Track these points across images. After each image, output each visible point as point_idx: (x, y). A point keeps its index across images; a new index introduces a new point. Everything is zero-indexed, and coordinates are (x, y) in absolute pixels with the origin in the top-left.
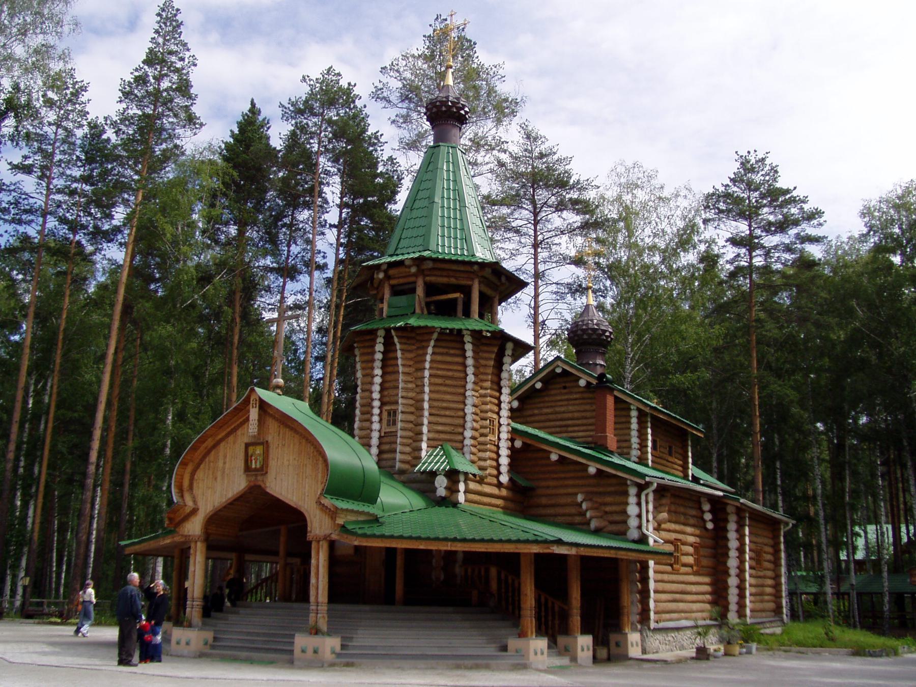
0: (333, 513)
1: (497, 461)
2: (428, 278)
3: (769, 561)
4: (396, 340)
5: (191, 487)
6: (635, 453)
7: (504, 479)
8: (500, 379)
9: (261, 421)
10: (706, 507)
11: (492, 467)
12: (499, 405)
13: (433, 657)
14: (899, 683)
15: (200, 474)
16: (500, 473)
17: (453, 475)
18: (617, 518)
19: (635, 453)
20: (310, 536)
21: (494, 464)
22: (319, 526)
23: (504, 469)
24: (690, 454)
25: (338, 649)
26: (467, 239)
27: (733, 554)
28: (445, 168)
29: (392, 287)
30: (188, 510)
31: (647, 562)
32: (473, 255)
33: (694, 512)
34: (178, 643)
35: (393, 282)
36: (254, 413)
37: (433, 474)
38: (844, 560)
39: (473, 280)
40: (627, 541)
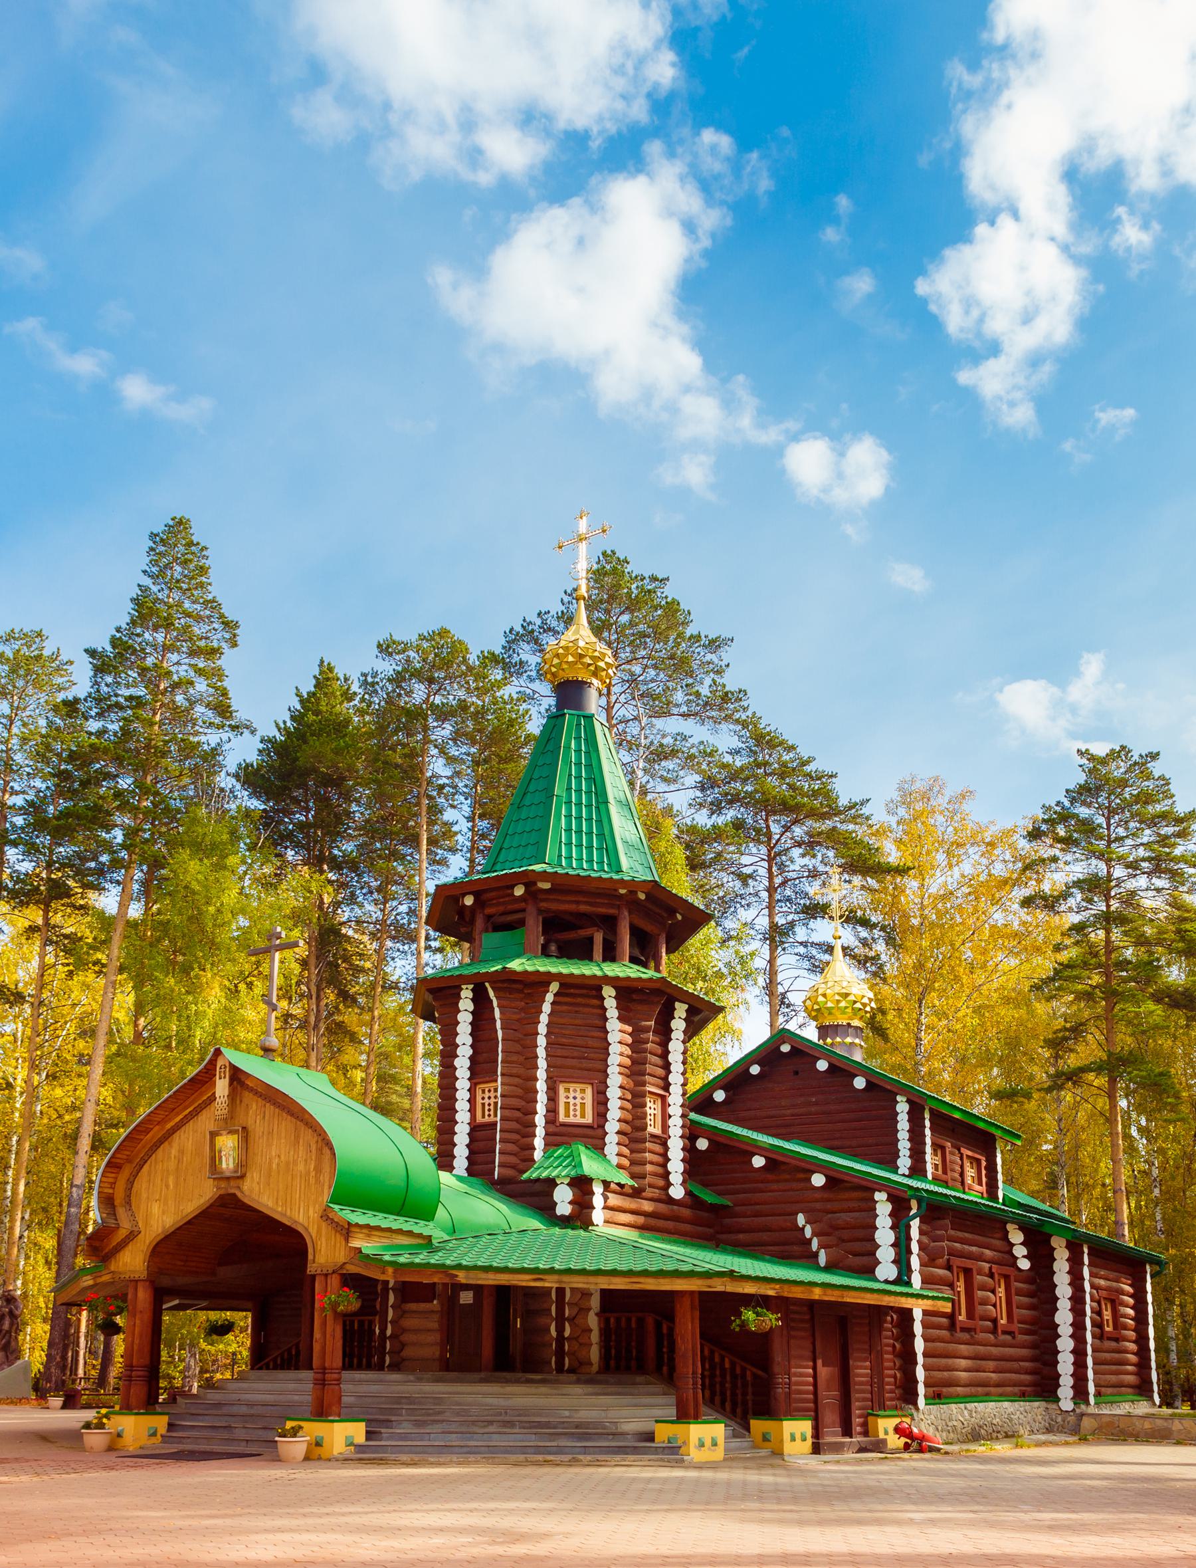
0: (347, 1230)
1: (664, 1166)
2: (544, 905)
3: (1126, 1316)
4: (491, 993)
5: (128, 1202)
6: (904, 1162)
7: (677, 1192)
9: (233, 1096)
10: (1016, 1237)
11: (655, 1174)
12: (666, 1087)
15: (141, 1184)
16: (669, 1184)
17: (581, 1184)
18: (857, 1246)
19: (904, 1162)
20: (311, 1269)
21: (660, 1170)
22: (325, 1253)
23: (676, 1178)
24: (927, 1123)
25: (360, 1439)
28: (573, 746)
29: (489, 918)
30: (122, 1233)
32: (620, 871)
33: (997, 1243)
34: (793, 1439)
35: (488, 911)
36: (222, 1087)
37: (551, 1183)
39: (619, 907)
40: (877, 1280)
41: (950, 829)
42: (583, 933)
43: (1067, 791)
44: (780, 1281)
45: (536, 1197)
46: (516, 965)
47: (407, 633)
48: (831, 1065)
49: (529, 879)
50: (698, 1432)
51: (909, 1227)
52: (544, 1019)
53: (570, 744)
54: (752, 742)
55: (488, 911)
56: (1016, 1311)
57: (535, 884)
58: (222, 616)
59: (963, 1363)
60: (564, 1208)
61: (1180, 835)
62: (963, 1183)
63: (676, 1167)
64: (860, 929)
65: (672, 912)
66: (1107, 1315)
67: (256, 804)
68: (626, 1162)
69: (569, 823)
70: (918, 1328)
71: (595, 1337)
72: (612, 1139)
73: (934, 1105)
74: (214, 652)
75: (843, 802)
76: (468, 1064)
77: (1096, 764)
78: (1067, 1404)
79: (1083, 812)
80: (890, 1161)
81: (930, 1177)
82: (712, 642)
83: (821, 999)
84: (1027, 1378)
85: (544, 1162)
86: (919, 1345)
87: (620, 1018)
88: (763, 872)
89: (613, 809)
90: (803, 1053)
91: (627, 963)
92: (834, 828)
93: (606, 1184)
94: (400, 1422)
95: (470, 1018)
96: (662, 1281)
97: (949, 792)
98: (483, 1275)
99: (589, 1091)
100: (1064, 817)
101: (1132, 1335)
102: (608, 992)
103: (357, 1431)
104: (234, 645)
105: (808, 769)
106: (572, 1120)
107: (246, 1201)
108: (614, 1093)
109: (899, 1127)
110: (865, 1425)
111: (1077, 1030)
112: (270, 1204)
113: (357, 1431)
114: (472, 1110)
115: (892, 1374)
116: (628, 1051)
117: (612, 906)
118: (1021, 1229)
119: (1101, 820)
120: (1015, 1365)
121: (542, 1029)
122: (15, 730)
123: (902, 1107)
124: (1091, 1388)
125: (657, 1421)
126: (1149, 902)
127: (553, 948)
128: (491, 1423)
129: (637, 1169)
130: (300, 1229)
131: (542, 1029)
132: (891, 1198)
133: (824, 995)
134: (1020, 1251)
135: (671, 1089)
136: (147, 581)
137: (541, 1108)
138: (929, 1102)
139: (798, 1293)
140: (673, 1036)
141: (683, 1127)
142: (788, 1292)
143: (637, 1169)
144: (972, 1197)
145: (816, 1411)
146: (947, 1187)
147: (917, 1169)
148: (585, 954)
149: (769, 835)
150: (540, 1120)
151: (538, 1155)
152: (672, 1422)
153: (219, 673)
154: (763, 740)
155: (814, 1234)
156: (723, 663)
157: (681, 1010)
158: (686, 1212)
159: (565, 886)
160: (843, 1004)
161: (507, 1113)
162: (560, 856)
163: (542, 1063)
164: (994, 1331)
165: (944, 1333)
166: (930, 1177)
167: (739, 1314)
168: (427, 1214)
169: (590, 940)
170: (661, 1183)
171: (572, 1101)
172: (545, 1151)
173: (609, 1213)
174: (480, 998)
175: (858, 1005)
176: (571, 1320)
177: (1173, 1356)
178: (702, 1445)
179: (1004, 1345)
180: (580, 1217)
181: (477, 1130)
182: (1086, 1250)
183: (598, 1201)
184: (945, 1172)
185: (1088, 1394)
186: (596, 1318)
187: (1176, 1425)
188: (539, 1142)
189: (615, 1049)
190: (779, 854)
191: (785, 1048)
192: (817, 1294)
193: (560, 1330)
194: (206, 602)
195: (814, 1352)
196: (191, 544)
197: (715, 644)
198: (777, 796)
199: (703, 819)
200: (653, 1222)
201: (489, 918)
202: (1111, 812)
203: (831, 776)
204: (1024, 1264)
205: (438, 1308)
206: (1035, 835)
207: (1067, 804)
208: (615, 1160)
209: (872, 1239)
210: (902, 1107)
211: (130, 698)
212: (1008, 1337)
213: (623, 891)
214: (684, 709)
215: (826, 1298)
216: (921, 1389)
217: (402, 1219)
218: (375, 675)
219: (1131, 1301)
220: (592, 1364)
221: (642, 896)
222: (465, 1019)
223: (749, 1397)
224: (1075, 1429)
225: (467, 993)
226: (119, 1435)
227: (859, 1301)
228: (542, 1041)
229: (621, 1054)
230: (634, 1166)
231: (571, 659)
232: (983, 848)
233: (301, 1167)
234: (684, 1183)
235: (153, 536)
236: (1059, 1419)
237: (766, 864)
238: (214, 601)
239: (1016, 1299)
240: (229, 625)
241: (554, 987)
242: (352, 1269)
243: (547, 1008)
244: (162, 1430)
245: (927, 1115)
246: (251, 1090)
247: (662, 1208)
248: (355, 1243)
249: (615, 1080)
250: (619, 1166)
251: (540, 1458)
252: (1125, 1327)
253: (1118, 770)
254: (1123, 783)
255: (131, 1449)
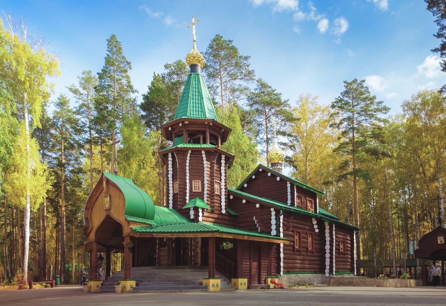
0: (129, 222)
1: (220, 204)
2: (187, 128)
6: (289, 202)
7: (224, 212)
8: (221, 170)
10: (315, 222)
11: (218, 206)
13: (167, 289)
14: (377, 304)
17: (196, 209)
19: (289, 202)
20: (124, 235)
22: (126, 231)
23: (223, 207)
24: (295, 190)
25: (134, 286)
26: (203, 111)
27: (328, 243)
30: (90, 228)
31: (280, 244)
33: (309, 224)
34: (241, 284)
35: (175, 132)
36: (104, 183)
37: (189, 209)
38: (412, 255)
40: (271, 235)
41: (313, 107)
42: (198, 136)
43: (341, 93)
44: (233, 234)
45: (184, 213)
46: (179, 146)
47: (171, 62)
48: (271, 174)
49: (183, 121)
50: (212, 281)
51: (280, 219)
52: (188, 161)
53: (193, 82)
54: (260, 86)
55: (175, 132)
56: (314, 245)
57: (184, 122)
58: (127, 61)
59: (298, 261)
60: (192, 217)
61: (371, 103)
62: (307, 208)
63: (223, 204)
64: (289, 137)
65: (221, 129)
66: (341, 246)
67: (144, 113)
68: (209, 203)
69: (193, 105)
70: (282, 250)
71: (199, 255)
72: (206, 196)
73: (297, 184)
74: (126, 71)
75: (283, 101)
76: (171, 176)
77: (348, 84)
78: (327, 275)
79: (346, 99)
80: (285, 202)
81: (296, 206)
82: (245, 58)
83: (271, 155)
84: (317, 266)
85: (189, 203)
86: (282, 255)
87: (207, 160)
88: (264, 123)
89: (205, 100)
90: (265, 171)
91: (209, 144)
92: (282, 109)
93: (203, 209)
94: (145, 281)
95: (171, 163)
96: (202, 234)
97: (312, 97)
98: (159, 234)
99: (200, 182)
100: (341, 101)
101: (350, 253)
102: (203, 152)
103: (133, 283)
104: (131, 69)
105: (275, 92)
106: (196, 191)
107: (111, 216)
108: (206, 182)
109: (288, 191)
110: (265, 280)
111: (346, 163)
112: (116, 217)
113: (133, 283)
114: (173, 190)
115: (274, 265)
116: (209, 170)
117: (204, 128)
118: (316, 220)
119: (351, 101)
120: (314, 262)
121: (188, 164)
122: (89, 98)
123: (289, 185)
124: (334, 269)
125: (204, 279)
126: (364, 124)
127: (192, 141)
128: (165, 280)
129: (212, 205)
130: (121, 224)
131: (188, 164)
132: (275, 210)
133: (272, 154)
134: (316, 227)
135: (222, 181)
136: (108, 53)
137: (188, 188)
138: (295, 183)
139: (240, 238)
140: (222, 165)
141: (225, 192)
142: (237, 237)
143: (212, 205)
144: (310, 212)
145: (250, 276)
146: (302, 209)
147: (293, 204)
148: (197, 142)
149: (266, 112)
150: (188, 191)
151: (187, 201)
152: (206, 279)
153: (128, 77)
154: (263, 85)
155: (257, 222)
156: (249, 63)
157: (223, 157)
158: (227, 218)
159: (193, 122)
160: (276, 157)
161: (180, 190)
162: (191, 114)
163: (188, 174)
164: (307, 252)
165: (291, 252)
166: (296, 206)
167: (223, 244)
168: (152, 218)
169: (200, 138)
170: (219, 209)
171: (196, 185)
172: (189, 200)
173: (205, 218)
174: (173, 157)
175: (280, 157)
176: (194, 250)
177: (375, 263)
178: (213, 286)
179: (310, 256)
180: (196, 220)
181: (175, 195)
182: (334, 226)
183: (200, 214)
184: (301, 205)
185: (333, 271)
186: (200, 250)
187: (355, 281)
188: (187, 198)
189: (206, 169)
190: (268, 118)
191: (261, 170)
192: (246, 238)
193: (191, 254)
194: (123, 57)
195: (250, 257)
196: (117, 42)
197: (246, 58)
198: (267, 101)
199: (248, 108)
200: (217, 221)
201: (175, 133)
202: (353, 98)
203: (280, 94)
204: (317, 231)
205: (167, 249)
206: (333, 106)
207: (341, 97)
208: (206, 202)
209: (271, 223)
210: (289, 185)
211: (108, 85)
212: (311, 253)
213: (206, 123)
214: (240, 77)
215: (249, 239)
216: (282, 269)
217: (144, 219)
218: (164, 74)
219: (350, 242)
220: (198, 263)
221: (211, 124)
222: (170, 163)
223: (232, 272)
224: (328, 283)
225: (170, 155)
226: (91, 287)
227: (260, 240)
228: (187, 168)
229: (207, 171)
230: (212, 203)
231: (192, 58)
232: (321, 112)
233: (121, 205)
234: (226, 209)
235: (107, 40)
236: (325, 280)
237: (265, 121)
238: (124, 57)
239: (314, 241)
240: (128, 63)
241: (190, 152)
242: (131, 234)
243: (188, 158)
244: (100, 286)
245: (295, 187)
246: (111, 184)
247: (220, 216)
248: (131, 226)
249: (206, 178)
250: (208, 204)
251: (173, 290)
252: (347, 250)
253: (355, 86)
254: (356, 90)
255: (93, 291)
